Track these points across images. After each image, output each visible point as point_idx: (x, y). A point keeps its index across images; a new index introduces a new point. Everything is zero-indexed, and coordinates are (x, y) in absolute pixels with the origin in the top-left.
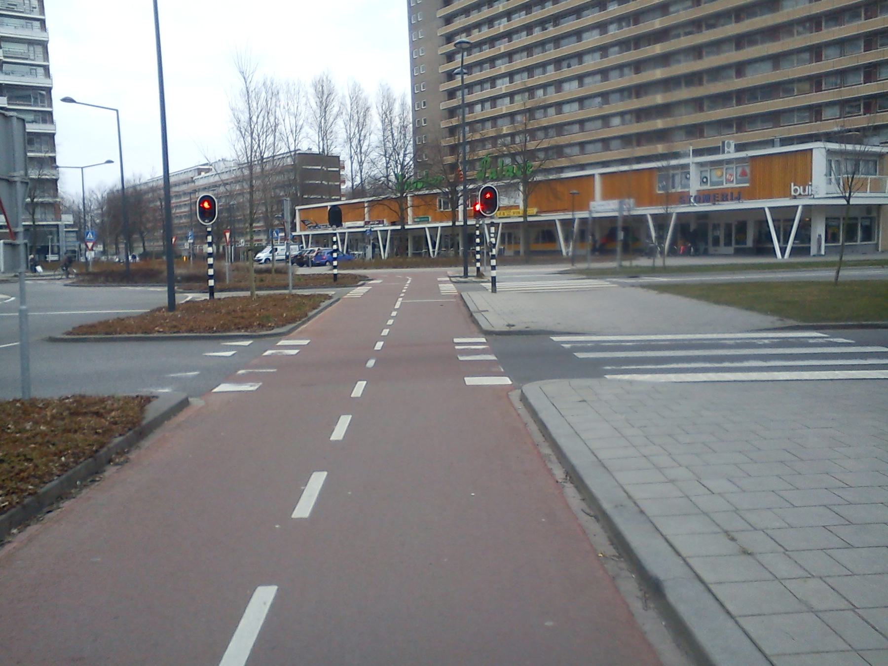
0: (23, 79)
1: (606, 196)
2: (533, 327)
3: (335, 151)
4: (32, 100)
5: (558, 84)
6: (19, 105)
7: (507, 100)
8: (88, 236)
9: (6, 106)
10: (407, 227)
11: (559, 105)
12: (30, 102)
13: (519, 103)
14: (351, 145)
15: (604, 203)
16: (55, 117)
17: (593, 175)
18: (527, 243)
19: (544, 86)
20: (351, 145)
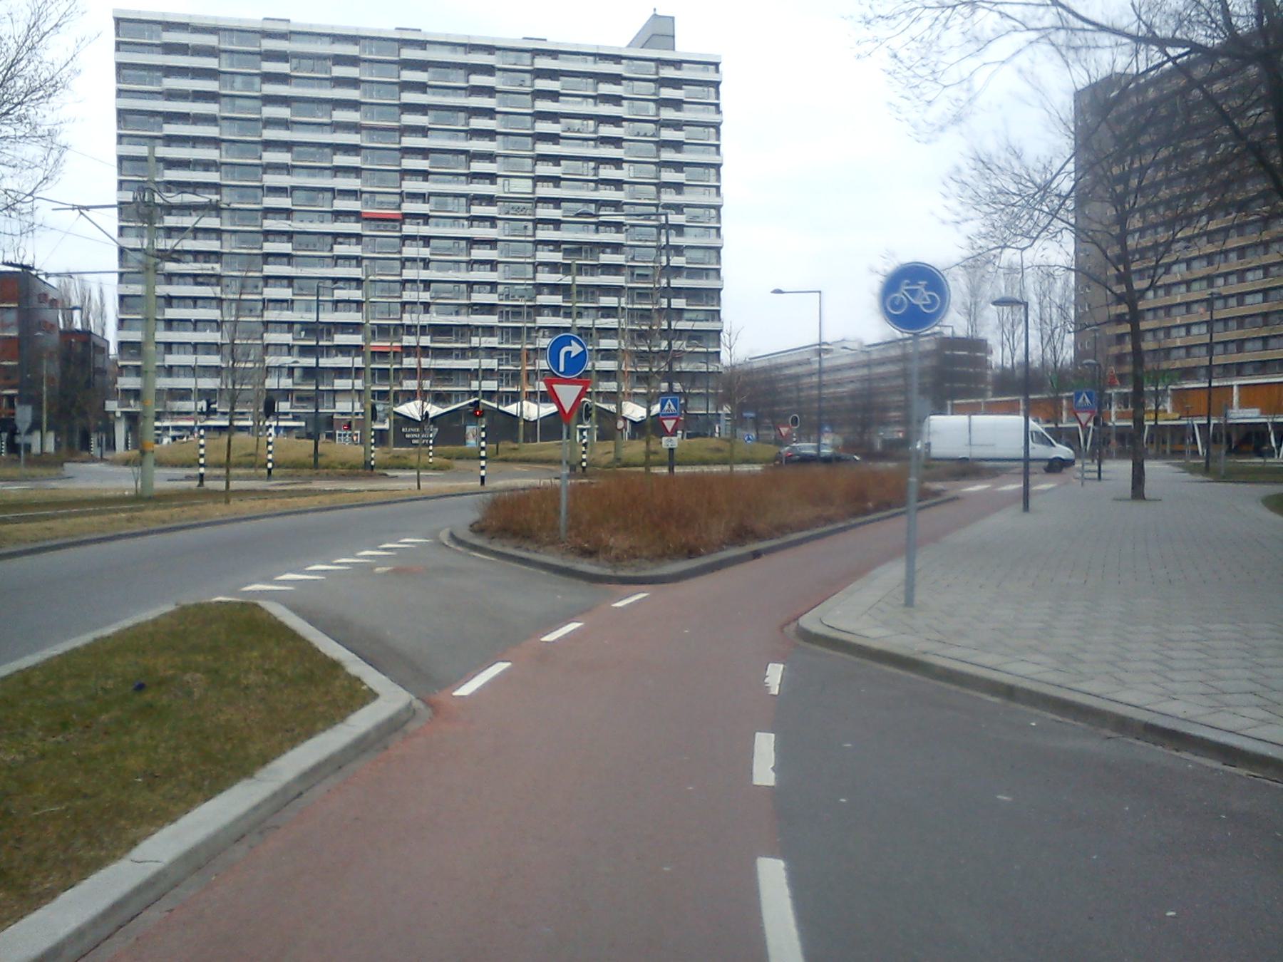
0: (578, 235)
1: (1243, 405)
2: (222, 24)
3: (981, 335)
4: (583, 254)
5: (1241, 274)
6: (693, 305)
7: (1183, 288)
8: (1081, 400)
9: (685, 307)
10: (1060, 425)
11: (1241, 297)
12: (581, 255)
13: (1200, 291)
14: (1003, 331)
15: (1241, 411)
16: (722, 315)
17: (1231, 387)
18: (1172, 444)
19: (1226, 275)
20: (1003, 331)
